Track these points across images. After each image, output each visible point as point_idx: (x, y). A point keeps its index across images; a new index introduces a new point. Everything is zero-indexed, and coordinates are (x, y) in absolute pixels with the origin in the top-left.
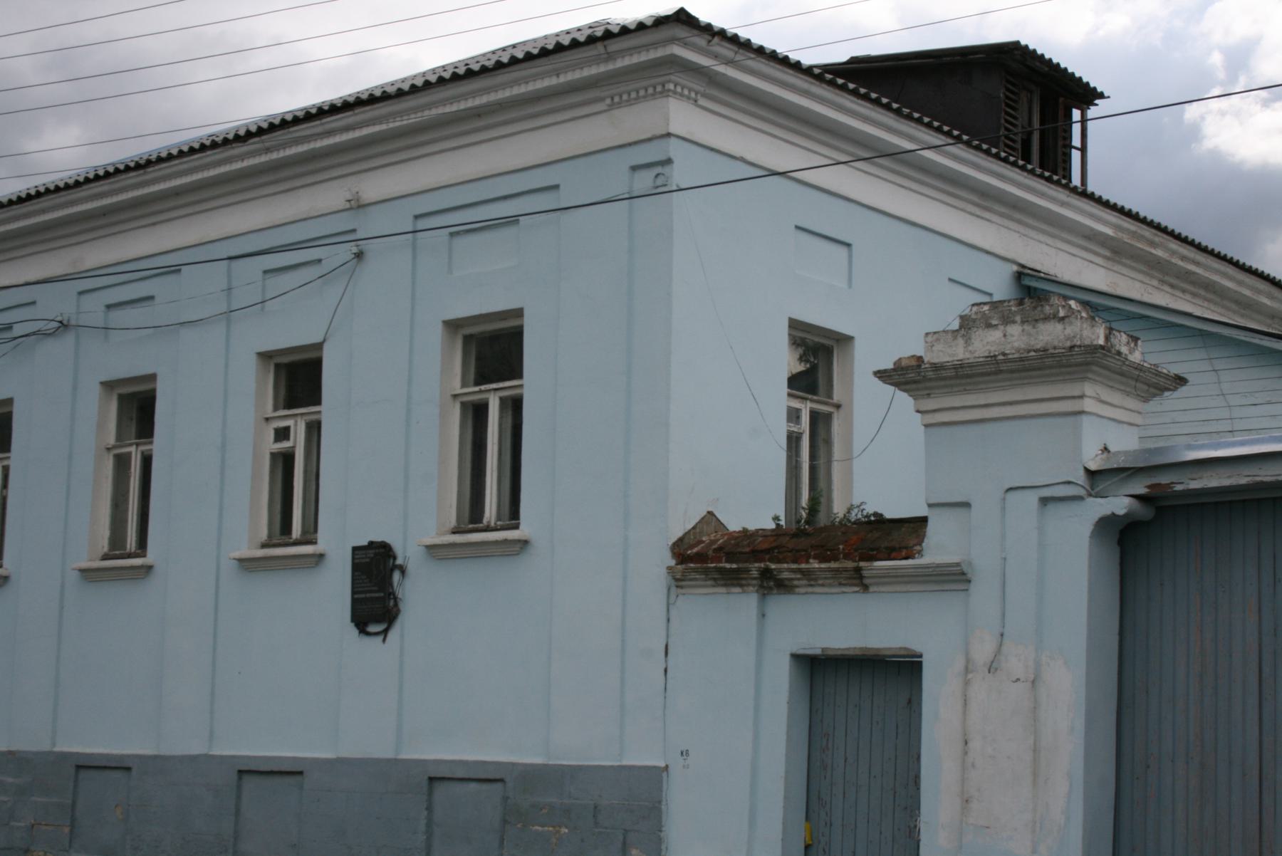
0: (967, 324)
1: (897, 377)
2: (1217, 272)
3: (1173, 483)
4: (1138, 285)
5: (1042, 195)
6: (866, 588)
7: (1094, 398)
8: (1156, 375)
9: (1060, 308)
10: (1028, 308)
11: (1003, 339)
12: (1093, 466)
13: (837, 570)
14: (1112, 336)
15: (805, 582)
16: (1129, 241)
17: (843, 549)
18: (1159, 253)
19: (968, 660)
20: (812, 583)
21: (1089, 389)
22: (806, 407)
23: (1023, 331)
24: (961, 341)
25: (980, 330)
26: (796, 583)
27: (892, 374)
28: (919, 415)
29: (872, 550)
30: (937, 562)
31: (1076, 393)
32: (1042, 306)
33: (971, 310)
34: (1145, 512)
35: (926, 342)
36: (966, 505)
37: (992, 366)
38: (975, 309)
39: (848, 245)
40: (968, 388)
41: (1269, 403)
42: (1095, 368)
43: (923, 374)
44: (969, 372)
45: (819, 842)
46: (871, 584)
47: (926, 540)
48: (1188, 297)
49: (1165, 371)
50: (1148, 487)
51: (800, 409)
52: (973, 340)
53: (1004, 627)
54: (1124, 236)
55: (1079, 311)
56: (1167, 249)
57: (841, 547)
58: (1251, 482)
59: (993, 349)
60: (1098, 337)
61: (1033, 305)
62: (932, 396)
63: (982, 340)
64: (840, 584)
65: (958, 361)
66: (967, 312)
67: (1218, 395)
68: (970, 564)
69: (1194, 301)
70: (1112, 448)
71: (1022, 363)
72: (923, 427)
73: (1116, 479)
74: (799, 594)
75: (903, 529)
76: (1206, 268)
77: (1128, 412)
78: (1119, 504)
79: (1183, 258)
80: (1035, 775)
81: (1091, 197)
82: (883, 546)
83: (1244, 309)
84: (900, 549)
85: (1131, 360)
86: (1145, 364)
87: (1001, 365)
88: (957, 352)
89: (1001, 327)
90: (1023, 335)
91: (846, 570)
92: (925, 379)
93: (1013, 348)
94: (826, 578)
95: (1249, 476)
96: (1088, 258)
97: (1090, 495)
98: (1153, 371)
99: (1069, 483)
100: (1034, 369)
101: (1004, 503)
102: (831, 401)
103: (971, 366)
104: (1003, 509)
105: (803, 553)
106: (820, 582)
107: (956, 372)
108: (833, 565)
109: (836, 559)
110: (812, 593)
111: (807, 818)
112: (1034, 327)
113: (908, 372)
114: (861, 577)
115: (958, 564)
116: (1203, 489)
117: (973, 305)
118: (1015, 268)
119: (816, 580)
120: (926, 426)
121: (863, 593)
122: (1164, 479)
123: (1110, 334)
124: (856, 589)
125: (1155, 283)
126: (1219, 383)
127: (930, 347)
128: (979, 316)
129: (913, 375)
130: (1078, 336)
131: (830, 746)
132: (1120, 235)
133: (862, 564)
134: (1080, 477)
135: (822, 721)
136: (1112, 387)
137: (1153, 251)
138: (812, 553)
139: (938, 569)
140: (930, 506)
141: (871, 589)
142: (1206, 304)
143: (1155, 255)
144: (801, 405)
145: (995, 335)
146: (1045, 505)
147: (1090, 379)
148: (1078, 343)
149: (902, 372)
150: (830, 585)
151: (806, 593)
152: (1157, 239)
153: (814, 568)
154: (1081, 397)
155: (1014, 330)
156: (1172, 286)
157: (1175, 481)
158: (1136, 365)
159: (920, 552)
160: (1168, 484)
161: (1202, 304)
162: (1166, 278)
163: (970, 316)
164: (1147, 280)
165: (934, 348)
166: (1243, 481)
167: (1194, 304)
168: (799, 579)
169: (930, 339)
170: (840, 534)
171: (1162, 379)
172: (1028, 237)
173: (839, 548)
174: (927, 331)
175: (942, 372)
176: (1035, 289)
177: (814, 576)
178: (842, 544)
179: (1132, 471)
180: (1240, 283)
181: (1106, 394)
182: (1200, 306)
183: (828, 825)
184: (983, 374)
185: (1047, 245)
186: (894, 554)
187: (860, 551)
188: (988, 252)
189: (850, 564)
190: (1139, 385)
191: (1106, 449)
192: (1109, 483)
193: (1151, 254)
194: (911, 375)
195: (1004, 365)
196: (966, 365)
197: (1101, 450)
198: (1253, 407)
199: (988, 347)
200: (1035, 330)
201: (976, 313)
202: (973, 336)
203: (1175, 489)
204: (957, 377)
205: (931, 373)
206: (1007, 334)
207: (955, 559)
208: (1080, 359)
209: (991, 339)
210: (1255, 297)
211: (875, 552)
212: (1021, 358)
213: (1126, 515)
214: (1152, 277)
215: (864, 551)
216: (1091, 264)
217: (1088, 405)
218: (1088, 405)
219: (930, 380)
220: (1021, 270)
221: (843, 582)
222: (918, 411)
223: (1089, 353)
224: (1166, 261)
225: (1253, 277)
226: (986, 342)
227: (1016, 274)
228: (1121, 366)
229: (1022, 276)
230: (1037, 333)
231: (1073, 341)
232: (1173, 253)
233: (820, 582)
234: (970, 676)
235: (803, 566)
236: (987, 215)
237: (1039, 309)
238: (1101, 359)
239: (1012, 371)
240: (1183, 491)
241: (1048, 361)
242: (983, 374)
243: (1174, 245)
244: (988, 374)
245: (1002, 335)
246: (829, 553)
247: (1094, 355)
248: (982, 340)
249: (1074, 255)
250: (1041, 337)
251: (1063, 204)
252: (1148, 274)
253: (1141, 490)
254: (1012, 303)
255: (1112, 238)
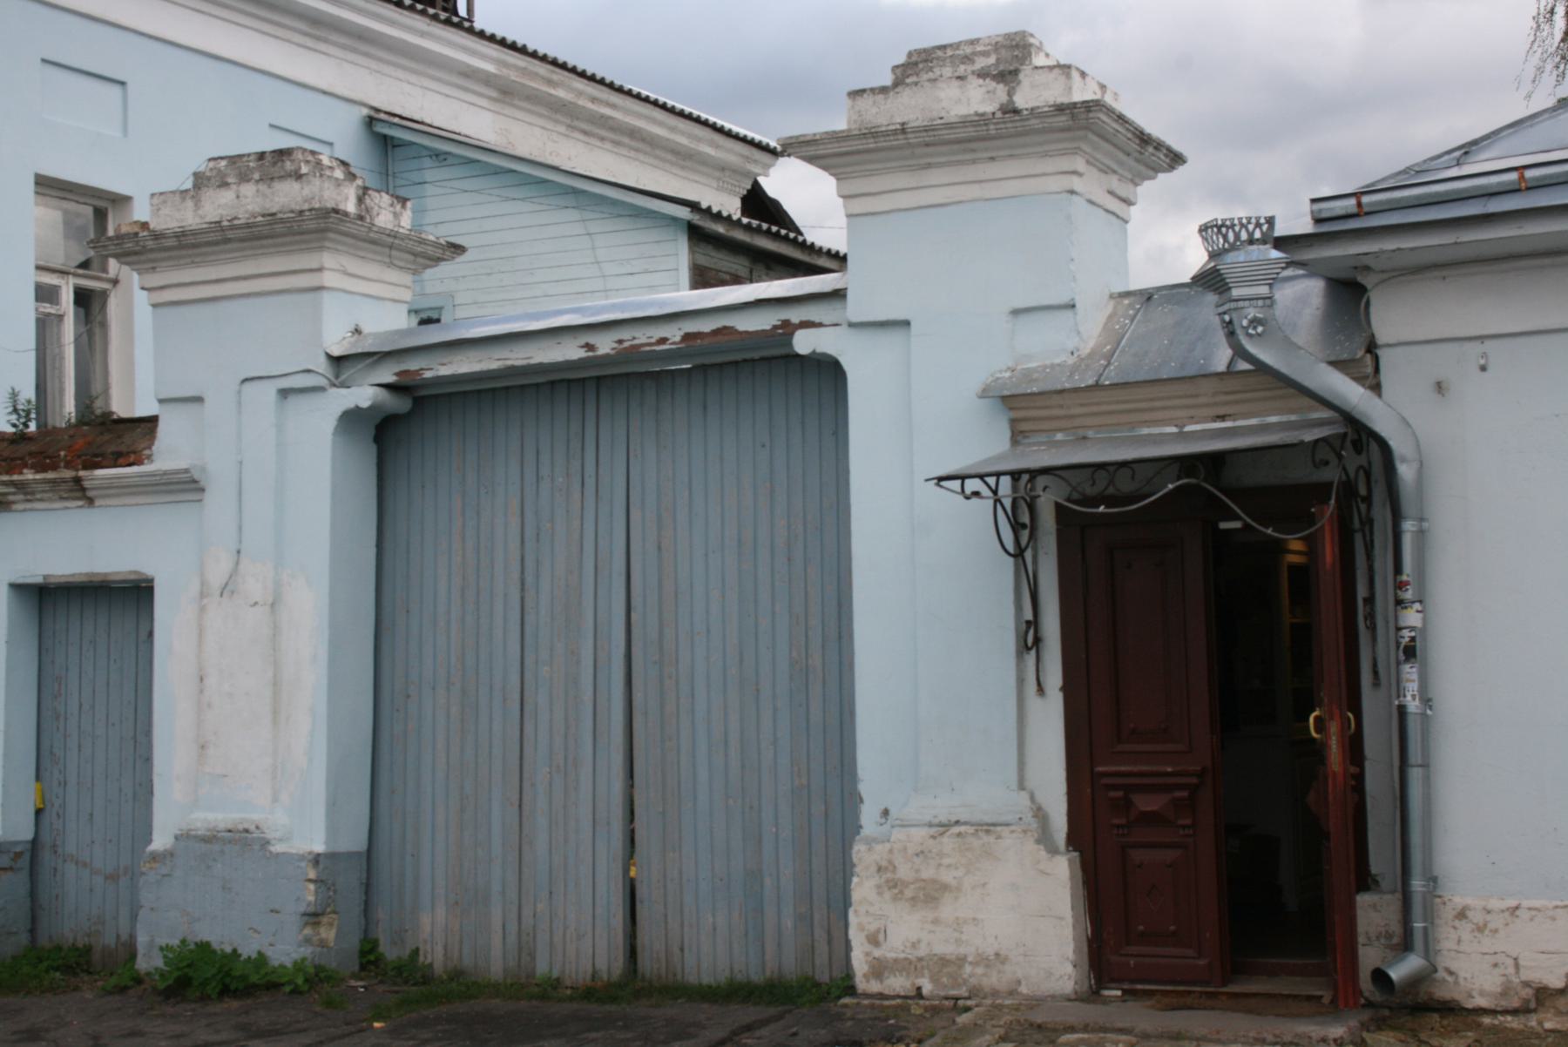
0: (200, 180)
1: (113, 247)
2: (639, 116)
3: (422, 369)
4: (537, 131)
5: (392, 23)
6: (90, 501)
7: (338, 271)
8: (420, 243)
9: (302, 164)
10: (267, 164)
11: (236, 201)
12: (336, 352)
13: (53, 482)
14: (366, 197)
15: (21, 497)
16: (518, 80)
17: (66, 456)
18: (561, 93)
19: (203, 584)
20: (29, 497)
21: (328, 259)
22: (67, 283)
23: (258, 191)
24: (190, 204)
25: (211, 190)
26: (11, 498)
27: (106, 243)
28: (145, 293)
29: (96, 456)
30: (164, 469)
31: (315, 265)
32: (283, 161)
33: (207, 166)
34: (401, 405)
35: (152, 205)
36: (198, 400)
37: (217, 234)
38: (211, 164)
39: (123, 83)
40: (197, 260)
41: (647, 272)
42: (331, 235)
43: (141, 243)
44: (193, 241)
45: (53, 805)
46: (96, 497)
47: (156, 443)
48: (608, 146)
49: (431, 238)
50: (397, 374)
51: (60, 287)
52: (203, 203)
53: (240, 542)
54: (511, 73)
55: (331, 168)
56: (570, 89)
57: (62, 453)
58: (502, 367)
59: (224, 213)
60: (347, 199)
61: (274, 160)
62: (158, 269)
63: (213, 203)
64: (62, 498)
65: (179, 227)
66: (202, 169)
67: (593, 263)
68: (203, 469)
69: (616, 150)
70: (367, 328)
71: (250, 230)
72: (151, 308)
73: (360, 366)
74: (16, 511)
75: (139, 430)
76: (627, 111)
77: (392, 287)
78: (364, 394)
79: (594, 100)
80: (275, 712)
81: (481, 35)
82: (110, 451)
83: (684, 160)
84: (128, 454)
85: (380, 225)
86: (401, 230)
87: (227, 233)
88: (188, 217)
89: (234, 187)
90: (258, 196)
91: (64, 481)
92: (143, 251)
93: (246, 212)
94: (43, 491)
95: (499, 360)
96: (466, 99)
97: (334, 385)
98: (415, 238)
99: (308, 371)
100: (267, 237)
101: (240, 397)
102: (104, 275)
103: (194, 233)
104: (239, 403)
105: (19, 462)
106: (38, 496)
107: (179, 241)
108: (50, 475)
109: (54, 468)
110: (31, 510)
111: (38, 778)
112: (269, 187)
113: (125, 241)
114: (83, 489)
115: (186, 471)
116: (453, 376)
117: (210, 160)
118: (365, 111)
119: (33, 493)
120: (155, 306)
121: (89, 507)
122: (413, 365)
123: (364, 194)
124: (80, 503)
125: (562, 129)
126: (593, 248)
127: (156, 210)
128: (214, 173)
129: (130, 245)
130: (317, 198)
131: (63, 692)
132: (505, 71)
133: (82, 473)
134: (322, 365)
135: (53, 662)
136: (363, 257)
137: (552, 91)
138: (30, 462)
139: (165, 477)
140: (161, 401)
141: (97, 503)
142: (632, 154)
143: (556, 97)
144: (59, 280)
145: (227, 196)
146: (286, 398)
147: (329, 248)
148: (317, 206)
149: (117, 242)
150: (50, 500)
151: (24, 510)
152: (555, 77)
153: (27, 480)
154: (320, 270)
155: (248, 190)
156: (585, 133)
157: (424, 367)
158: (387, 232)
159: (149, 457)
160: (417, 371)
161: (628, 154)
162: (576, 123)
163: (204, 173)
164: (550, 125)
165: (160, 212)
166: (494, 365)
167: (616, 153)
168: (14, 494)
169: (155, 201)
170: (66, 437)
171: (429, 248)
172: (383, 74)
173: (59, 455)
174: (151, 192)
175: (163, 241)
176: (392, 138)
177: (29, 490)
178: (64, 450)
179: (379, 356)
180: (673, 129)
181: (353, 265)
182: (624, 156)
183: (63, 784)
184: (209, 244)
185: (409, 83)
186: (121, 461)
187: (84, 458)
188: (325, 93)
189: (68, 474)
190: (394, 253)
191: (357, 331)
192: (352, 371)
193: (551, 95)
194: (129, 245)
195: (231, 232)
196: (188, 233)
197: (351, 332)
198: (630, 276)
199: (220, 211)
200: (271, 190)
201: (211, 169)
202: (203, 199)
203: (425, 376)
204: (181, 247)
205: (151, 243)
206: (241, 195)
207: (183, 465)
208: (312, 225)
209: (223, 201)
210: (693, 146)
211: (100, 459)
212: (248, 224)
213: (370, 408)
214: (557, 122)
215: (88, 457)
216: (472, 107)
217: (329, 279)
218: (329, 279)
219: (152, 250)
220: (372, 113)
221: (65, 495)
222: (143, 288)
223: (321, 218)
224: (571, 103)
225: (688, 122)
226: (220, 205)
227: (367, 119)
228: (368, 232)
229: (374, 122)
230: (273, 194)
231: (311, 203)
232: (580, 94)
233: (38, 496)
234: (205, 601)
235: (15, 477)
236: (322, 47)
237: (279, 164)
238: (337, 224)
239: (242, 240)
240: (433, 378)
241: (279, 228)
242: (209, 244)
243: (580, 84)
244: (216, 243)
245: (234, 196)
246: (48, 461)
247: (327, 221)
248: (213, 203)
249: (447, 96)
250: (277, 199)
251: (423, 34)
252: (549, 118)
253: (390, 378)
254: (252, 158)
255: (495, 75)
